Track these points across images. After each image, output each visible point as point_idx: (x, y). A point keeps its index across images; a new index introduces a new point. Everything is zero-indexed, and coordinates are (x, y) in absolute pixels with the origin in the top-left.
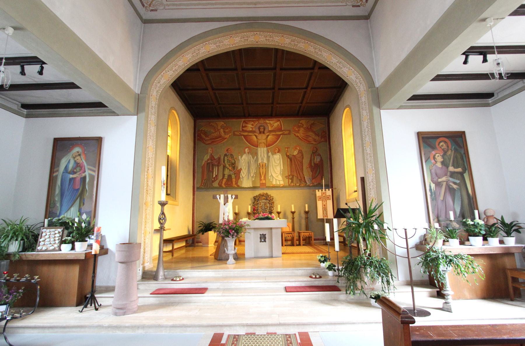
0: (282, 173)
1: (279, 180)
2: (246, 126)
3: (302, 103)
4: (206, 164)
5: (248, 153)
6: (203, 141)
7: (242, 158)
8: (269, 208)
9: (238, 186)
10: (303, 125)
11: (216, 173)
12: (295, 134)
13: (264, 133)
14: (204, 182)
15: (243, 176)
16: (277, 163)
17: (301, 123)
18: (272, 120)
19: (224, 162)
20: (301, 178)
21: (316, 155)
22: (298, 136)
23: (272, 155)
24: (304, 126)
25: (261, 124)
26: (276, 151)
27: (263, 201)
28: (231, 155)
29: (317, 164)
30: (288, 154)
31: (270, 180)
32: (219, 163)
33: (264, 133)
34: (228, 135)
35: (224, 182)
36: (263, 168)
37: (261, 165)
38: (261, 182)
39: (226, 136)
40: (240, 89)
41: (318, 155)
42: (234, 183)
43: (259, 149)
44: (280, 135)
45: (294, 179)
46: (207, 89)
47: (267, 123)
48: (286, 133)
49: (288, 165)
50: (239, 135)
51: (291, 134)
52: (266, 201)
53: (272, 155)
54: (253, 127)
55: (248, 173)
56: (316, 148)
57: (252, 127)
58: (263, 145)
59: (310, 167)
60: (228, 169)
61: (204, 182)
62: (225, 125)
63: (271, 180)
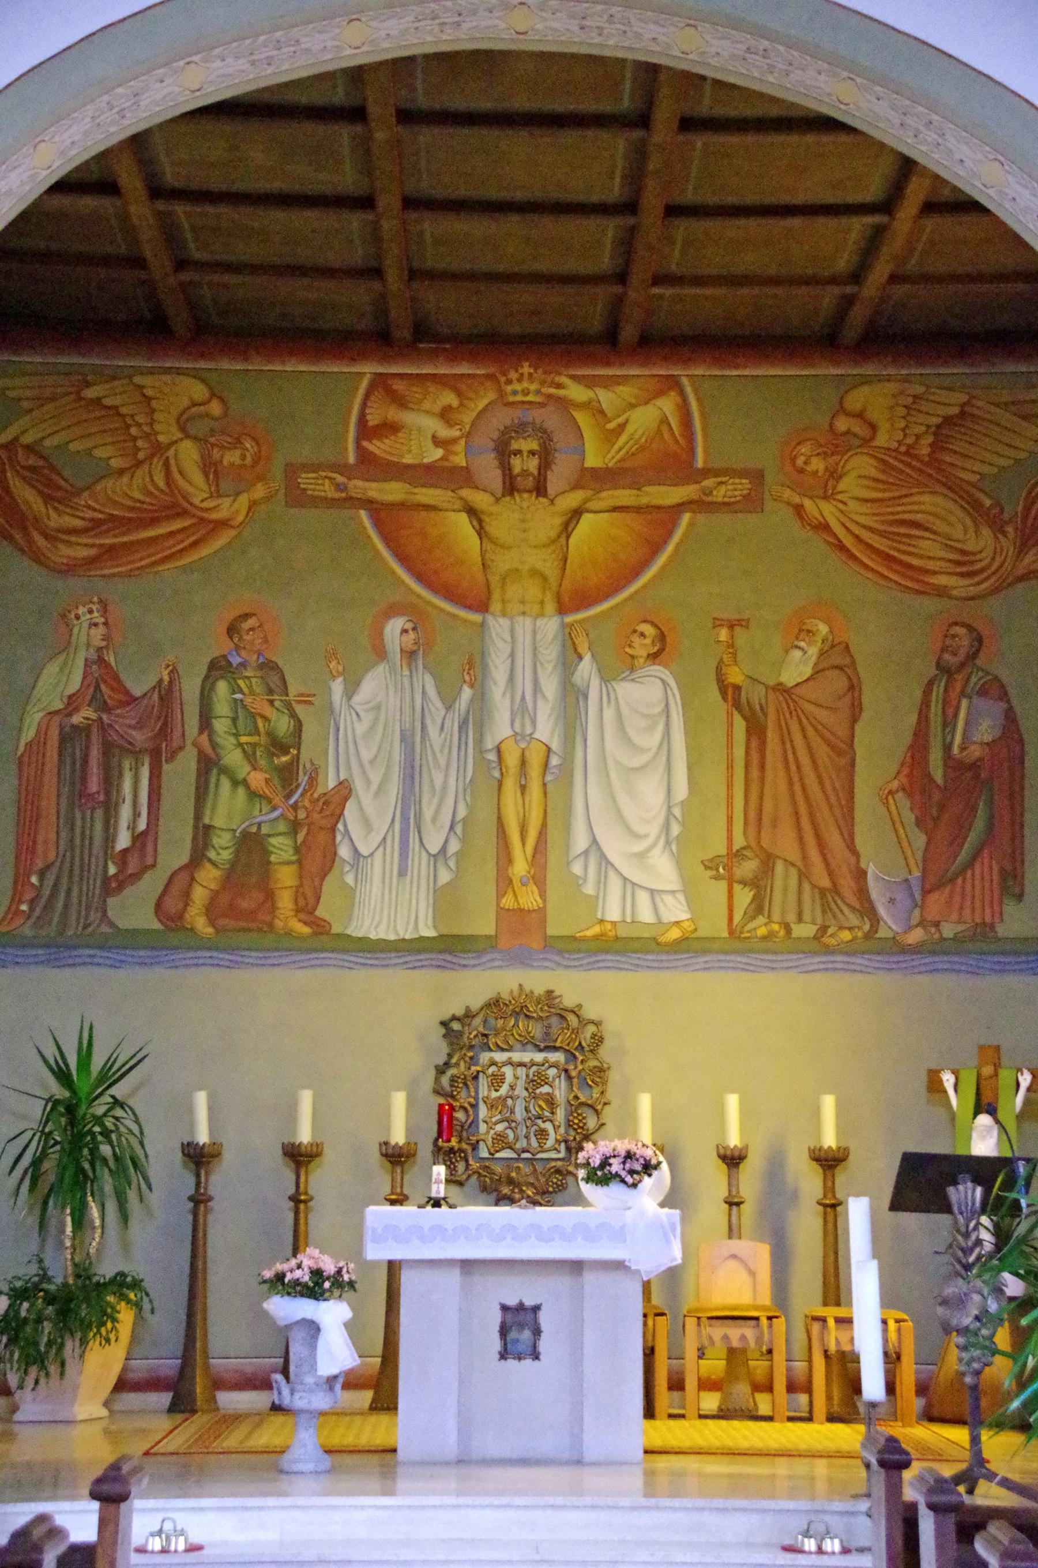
0: (676, 830)
1: (652, 892)
2: (391, 428)
3: (856, 277)
4: (54, 734)
5: (410, 655)
6: (30, 542)
7: (357, 699)
8: (569, 1113)
9: (320, 927)
10: (873, 427)
11: (136, 815)
12: (799, 509)
13: (540, 489)
14: (39, 889)
15: (364, 851)
16: (642, 750)
17: (860, 415)
18: (608, 382)
19: (206, 723)
20: (831, 874)
21: (963, 694)
22: (824, 527)
23: (607, 677)
24: (882, 439)
25: (517, 413)
26: (641, 648)
27: (516, 1056)
28: (269, 667)
29: (974, 766)
30: (735, 676)
31: (577, 882)
32: (164, 733)
33: (540, 489)
34: (243, 500)
35: (200, 895)
36: (523, 788)
37: (512, 760)
38: (508, 902)
39: (225, 508)
40: (366, 202)
41: (983, 692)
42: (285, 902)
43: (498, 626)
44: (679, 508)
45: (778, 883)
46: (138, 262)
47: (564, 404)
48: (719, 495)
49: (730, 766)
50: (331, 503)
51: (769, 505)
52: (539, 1057)
53: (607, 677)
54: (455, 433)
55: (405, 818)
56: (970, 628)
57: (445, 432)
58: (533, 591)
59: (909, 793)
60: (235, 783)
61: (39, 889)
62: (215, 408)
63: (589, 889)
